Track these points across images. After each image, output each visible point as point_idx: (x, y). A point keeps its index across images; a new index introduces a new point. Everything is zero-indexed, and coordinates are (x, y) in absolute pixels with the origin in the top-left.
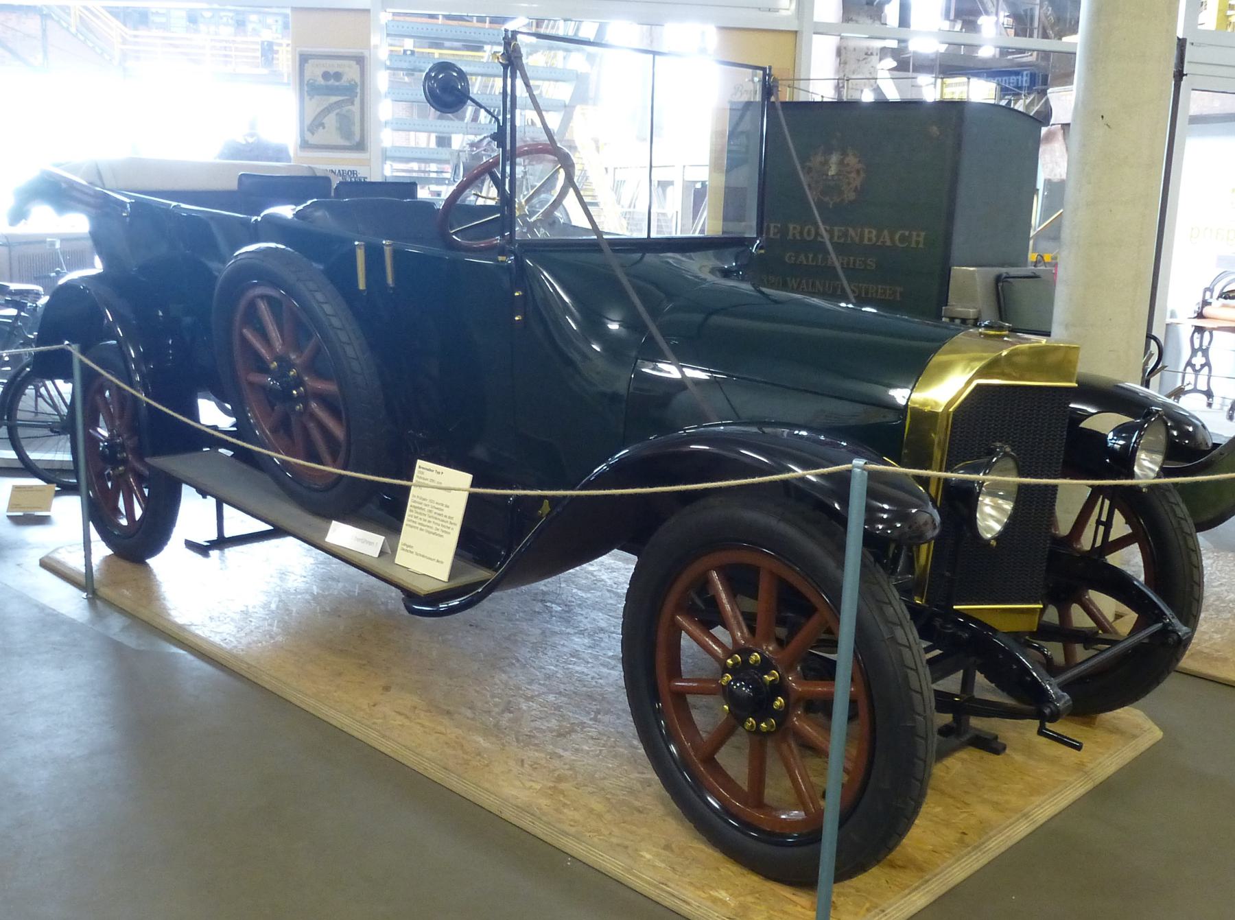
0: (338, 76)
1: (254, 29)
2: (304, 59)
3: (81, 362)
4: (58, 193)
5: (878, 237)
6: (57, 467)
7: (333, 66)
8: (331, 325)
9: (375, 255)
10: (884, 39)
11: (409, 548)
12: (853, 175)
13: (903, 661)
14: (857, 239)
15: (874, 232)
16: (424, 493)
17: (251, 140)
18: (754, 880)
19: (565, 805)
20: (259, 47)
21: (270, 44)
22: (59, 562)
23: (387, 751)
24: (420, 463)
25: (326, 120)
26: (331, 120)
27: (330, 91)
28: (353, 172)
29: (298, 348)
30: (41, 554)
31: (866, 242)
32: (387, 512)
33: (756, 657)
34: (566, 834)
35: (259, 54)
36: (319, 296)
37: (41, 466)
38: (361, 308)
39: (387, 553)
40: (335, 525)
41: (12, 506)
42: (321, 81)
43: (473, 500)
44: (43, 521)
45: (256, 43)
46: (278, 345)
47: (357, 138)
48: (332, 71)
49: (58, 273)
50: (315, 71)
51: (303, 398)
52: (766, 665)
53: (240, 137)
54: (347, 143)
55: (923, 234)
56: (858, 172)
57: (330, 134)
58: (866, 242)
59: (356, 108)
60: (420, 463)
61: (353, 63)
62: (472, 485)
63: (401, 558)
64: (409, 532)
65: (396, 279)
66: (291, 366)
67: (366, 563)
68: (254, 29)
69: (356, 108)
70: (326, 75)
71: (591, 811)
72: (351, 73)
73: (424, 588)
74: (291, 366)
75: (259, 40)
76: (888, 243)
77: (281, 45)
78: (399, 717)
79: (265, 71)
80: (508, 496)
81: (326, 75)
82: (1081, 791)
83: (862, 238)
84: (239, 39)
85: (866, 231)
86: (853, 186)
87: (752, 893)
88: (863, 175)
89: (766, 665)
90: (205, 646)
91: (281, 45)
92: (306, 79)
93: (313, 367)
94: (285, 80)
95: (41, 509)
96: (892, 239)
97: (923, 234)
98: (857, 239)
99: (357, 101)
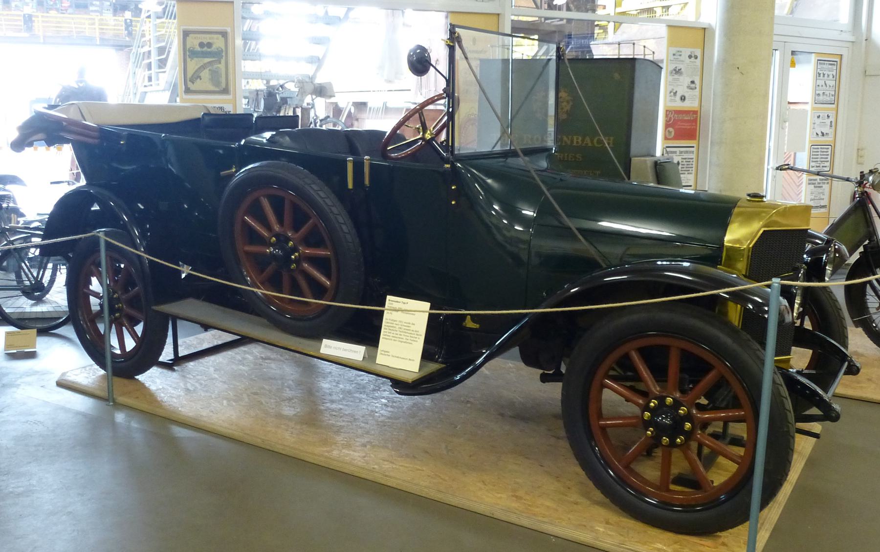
0: (209, 45)
1: (16, 6)
2: (186, 34)
3: (106, 242)
4: (44, 130)
5: (583, 141)
6: (34, 316)
7: (206, 39)
8: (332, 212)
9: (358, 167)
10: (518, 16)
11: (386, 353)
12: (565, 103)
13: (780, 393)
14: (569, 142)
15: (580, 138)
16: (396, 316)
17: (81, 85)
18: (670, 535)
19: (529, 505)
20: (22, 18)
21: (30, 16)
22: (73, 382)
23: (394, 485)
24: (389, 297)
25: (202, 74)
26: (205, 74)
27: (204, 55)
28: (221, 108)
29: (296, 229)
30: (56, 377)
31: (575, 144)
32: (366, 331)
33: (669, 400)
34: (544, 522)
35: (123, 28)
36: (322, 194)
37: (14, 317)
38: (355, 203)
39: (371, 358)
40: (325, 342)
41: (7, 346)
42: (198, 49)
43: (432, 318)
44: (32, 355)
45: (19, 16)
46: (277, 228)
47: (223, 85)
48: (205, 41)
49: (457, 195)
50: (194, 42)
51: (297, 261)
52: (677, 404)
53: (72, 82)
54: (217, 89)
55: (612, 138)
56: (568, 102)
57: (205, 82)
58: (575, 144)
59: (222, 66)
60: (389, 297)
61: (220, 36)
62: (431, 309)
63: (381, 359)
64: (384, 343)
65: (370, 181)
66: (288, 239)
67: (358, 365)
68: (16, 6)
69: (222, 66)
70: (201, 45)
71: (548, 507)
72: (218, 43)
73: (409, 378)
74: (288, 239)
75: (22, 14)
76: (590, 145)
77: (37, 17)
78: (386, 463)
79: (26, 35)
80: (440, 315)
81: (201, 45)
82: (803, 464)
83: (572, 141)
84: (5, 13)
85: (575, 137)
86: (565, 110)
87: (676, 543)
88: (571, 103)
89: (677, 404)
90: (219, 429)
91: (37, 17)
92: (188, 47)
93: (308, 241)
94: (98, 43)
95: (28, 347)
96: (592, 142)
97: (612, 138)
98: (569, 142)
99: (223, 61)
